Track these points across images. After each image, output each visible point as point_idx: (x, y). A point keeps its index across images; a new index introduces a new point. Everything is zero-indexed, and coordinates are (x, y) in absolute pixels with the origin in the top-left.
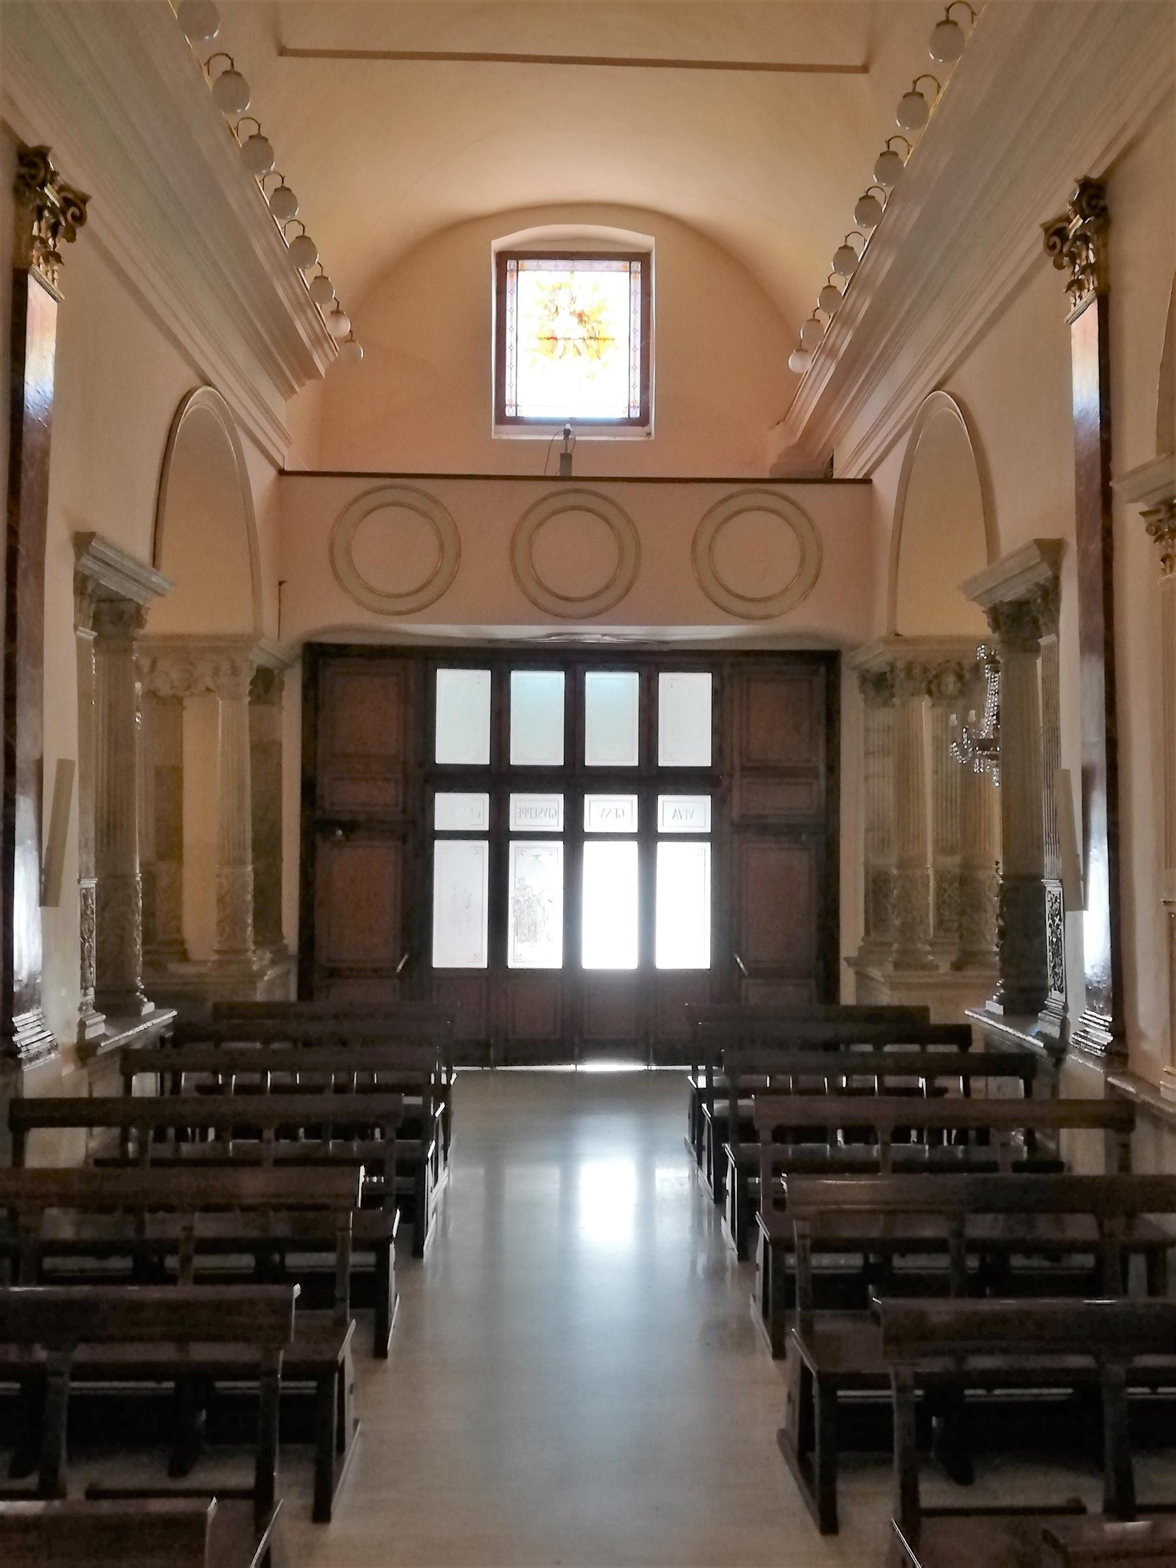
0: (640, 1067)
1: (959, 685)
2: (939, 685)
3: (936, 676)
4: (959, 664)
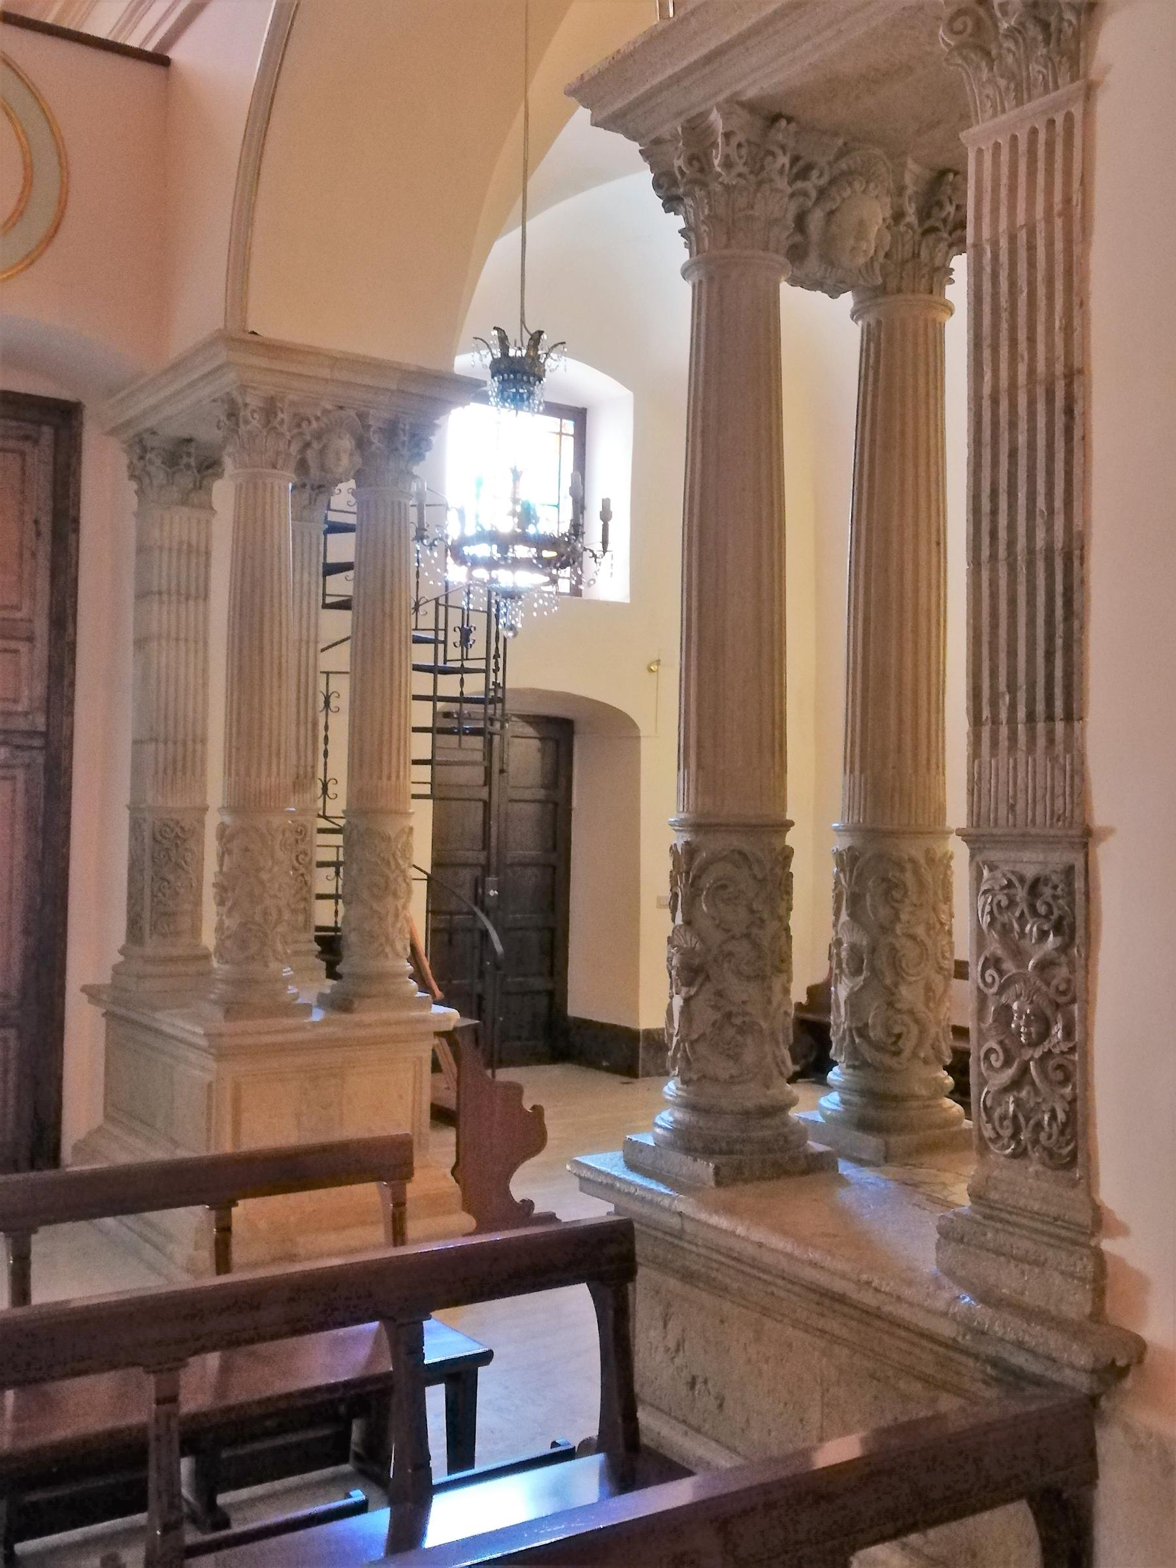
0: (666, 1191)
1: (358, 459)
2: (322, 452)
3: (318, 436)
4: (362, 416)
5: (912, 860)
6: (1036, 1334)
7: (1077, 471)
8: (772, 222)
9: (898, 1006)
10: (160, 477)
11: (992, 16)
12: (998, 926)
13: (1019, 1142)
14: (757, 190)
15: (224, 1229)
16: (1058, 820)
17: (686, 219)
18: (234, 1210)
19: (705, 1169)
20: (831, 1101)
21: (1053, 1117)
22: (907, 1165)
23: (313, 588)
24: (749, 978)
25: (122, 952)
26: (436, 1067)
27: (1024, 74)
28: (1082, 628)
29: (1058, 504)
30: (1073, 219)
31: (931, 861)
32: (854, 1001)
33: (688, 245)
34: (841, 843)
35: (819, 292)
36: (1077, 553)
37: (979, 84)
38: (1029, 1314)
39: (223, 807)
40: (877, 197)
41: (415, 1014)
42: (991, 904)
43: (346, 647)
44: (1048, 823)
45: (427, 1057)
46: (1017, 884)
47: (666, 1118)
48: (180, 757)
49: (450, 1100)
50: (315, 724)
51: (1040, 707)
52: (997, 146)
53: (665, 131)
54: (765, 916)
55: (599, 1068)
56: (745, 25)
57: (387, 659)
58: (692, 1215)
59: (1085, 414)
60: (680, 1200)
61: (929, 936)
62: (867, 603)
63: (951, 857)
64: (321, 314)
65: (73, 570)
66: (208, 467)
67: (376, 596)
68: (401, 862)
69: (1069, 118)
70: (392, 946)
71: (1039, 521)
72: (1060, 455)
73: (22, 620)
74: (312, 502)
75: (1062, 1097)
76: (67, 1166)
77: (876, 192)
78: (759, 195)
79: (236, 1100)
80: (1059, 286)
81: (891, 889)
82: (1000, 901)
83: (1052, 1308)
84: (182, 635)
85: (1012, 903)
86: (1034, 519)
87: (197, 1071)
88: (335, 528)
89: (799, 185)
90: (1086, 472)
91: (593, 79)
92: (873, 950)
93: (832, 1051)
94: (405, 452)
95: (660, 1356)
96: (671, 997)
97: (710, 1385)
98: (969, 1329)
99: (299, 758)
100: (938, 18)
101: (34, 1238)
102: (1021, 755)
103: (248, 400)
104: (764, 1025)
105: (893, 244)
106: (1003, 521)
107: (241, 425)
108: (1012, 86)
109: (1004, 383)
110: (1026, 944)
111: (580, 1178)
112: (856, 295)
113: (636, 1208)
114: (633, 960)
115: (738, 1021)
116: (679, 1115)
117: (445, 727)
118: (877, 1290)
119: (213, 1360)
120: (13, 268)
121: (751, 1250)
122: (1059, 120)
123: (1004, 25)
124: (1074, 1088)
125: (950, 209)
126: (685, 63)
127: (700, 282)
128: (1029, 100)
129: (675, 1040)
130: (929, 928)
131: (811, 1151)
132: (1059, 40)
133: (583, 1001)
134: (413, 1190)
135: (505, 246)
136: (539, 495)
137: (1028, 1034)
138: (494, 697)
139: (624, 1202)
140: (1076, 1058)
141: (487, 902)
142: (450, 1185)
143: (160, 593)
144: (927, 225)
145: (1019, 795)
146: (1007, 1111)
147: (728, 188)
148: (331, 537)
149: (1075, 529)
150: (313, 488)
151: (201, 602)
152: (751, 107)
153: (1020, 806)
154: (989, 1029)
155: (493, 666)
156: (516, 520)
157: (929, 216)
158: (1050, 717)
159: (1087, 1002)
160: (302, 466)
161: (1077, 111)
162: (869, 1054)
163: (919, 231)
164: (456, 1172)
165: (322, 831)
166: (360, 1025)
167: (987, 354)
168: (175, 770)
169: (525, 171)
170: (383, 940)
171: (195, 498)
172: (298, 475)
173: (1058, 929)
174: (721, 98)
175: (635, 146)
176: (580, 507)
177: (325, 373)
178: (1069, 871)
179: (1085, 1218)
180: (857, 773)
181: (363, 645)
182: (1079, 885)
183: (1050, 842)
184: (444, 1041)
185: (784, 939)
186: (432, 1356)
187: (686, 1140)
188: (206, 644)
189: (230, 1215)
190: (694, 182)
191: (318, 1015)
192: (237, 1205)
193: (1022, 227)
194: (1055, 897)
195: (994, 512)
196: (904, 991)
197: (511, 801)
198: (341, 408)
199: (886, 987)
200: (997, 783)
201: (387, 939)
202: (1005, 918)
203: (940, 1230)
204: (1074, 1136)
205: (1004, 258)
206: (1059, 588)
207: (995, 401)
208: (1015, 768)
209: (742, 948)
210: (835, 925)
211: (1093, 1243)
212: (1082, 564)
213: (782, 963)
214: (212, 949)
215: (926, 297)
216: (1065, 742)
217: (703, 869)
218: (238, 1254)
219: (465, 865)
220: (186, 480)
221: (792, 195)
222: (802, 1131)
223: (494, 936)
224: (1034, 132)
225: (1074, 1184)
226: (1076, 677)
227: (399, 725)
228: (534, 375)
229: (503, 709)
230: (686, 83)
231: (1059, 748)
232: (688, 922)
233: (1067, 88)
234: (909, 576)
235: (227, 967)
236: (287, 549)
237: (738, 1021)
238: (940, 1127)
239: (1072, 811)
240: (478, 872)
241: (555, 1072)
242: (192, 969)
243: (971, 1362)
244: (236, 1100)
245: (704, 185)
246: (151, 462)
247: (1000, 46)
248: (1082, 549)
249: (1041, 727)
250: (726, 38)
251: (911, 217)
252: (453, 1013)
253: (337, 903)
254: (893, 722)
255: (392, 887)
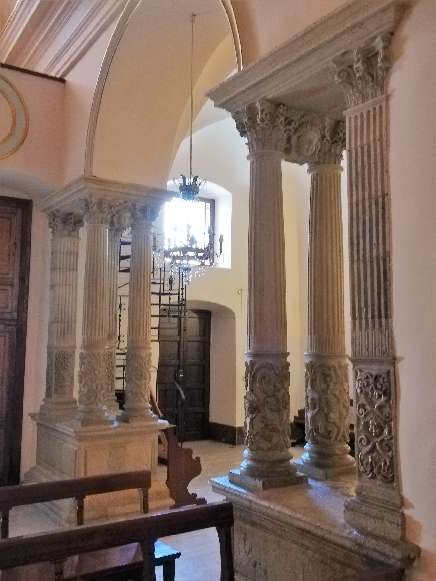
2: (119, 218)
3: (118, 212)
4: (134, 205)
5: (334, 367)
6: (380, 546)
7: (387, 230)
8: (278, 141)
9: (330, 421)
10: (60, 227)
11: (353, 71)
12: (364, 392)
13: (373, 473)
14: (273, 130)
15: (81, 507)
16: (384, 354)
17: (248, 139)
18: (84, 499)
19: (259, 483)
20: (306, 456)
21: (385, 463)
22: (334, 480)
23: (116, 266)
24: (274, 411)
25: (44, 400)
26: (160, 442)
27: (365, 92)
28: (390, 285)
29: (381, 241)
30: (383, 142)
31: (340, 366)
32: (313, 418)
33: (249, 148)
34: (308, 360)
35: (296, 164)
36: (388, 258)
37: (350, 95)
38: (378, 538)
39: (82, 347)
40: (316, 131)
41: (153, 423)
42: (361, 384)
43: (127, 286)
44: (380, 355)
45: (157, 438)
46: (370, 377)
47: (244, 464)
48: (66, 328)
49: (165, 455)
50: (116, 315)
51: (376, 313)
52: (356, 117)
53: (240, 109)
54: (280, 388)
55: (221, 441)
56: (268, 74)
57: (142, 292)
58: (254, 501)
59: (389, 209)
60: (251, 495)
61: (340, 394)
62: (315, 273)
63: (348, 365)
64: (118, 169)
65: (28, 261)
66: (78, 223)
67: (138, 270)
68: (147, 366)
69: (381, 107)
70: (144, 398)
71: (374, 247)
72: (381, 224)
73: (9, 279)
74: (115, 235)
75: (389, 456)
76: (23, 482)
77: (315, 130)
78: (273, 131)
79: (86, 458)
80: (379, 164)
81: (326, 377)
82: (364, 384)
83: (387, 536)
84: (68, 283)
85: (368, 384)
86: (372, 245)
87: (71, 445)
88: (124, 243)
89: (287, 127)
90: (390, 229)
91: (215, 91)
92: (320, 399)
93: (306, 438)
94: (149, 217)
95: (243, 554)
96: (246, 418)
97: (261, 565)
98: (357, 544)
99: (110, 328)
100: (335, 72)
101: (10, 511)
102: (370, 330)
103: (93, 200)
104: (280, 429)
105: (322, 147)
106: (361, 247)
107: (90, 209)
108: (361, 96)
109: (360, 198)
110: (373, 399)
111: (212, 486)
112: (309, 164)
113: (233, 498)
114: (232, 405)
115: (270, 427)
116: (249, 462)
117: (165, 313)
118: (322, 529)
119: (76, 558)
120: (7, 154)
121: (276, 514)
122: (378, 107)
123: (358, 75)
124: (392, 452)
125: (341, 134)
126: (247, 86)
127: (253, 161)
128: (367, 101)
129: (247, 434)
130: (340, 391)
131: (298, 476)
132: (376, 81)
133: (216, 416)
134: (150, 491)
135: (186, 142)
136: (198, 228)
137: (375, 433)
138: (182, 304)
139: (229, 495)
140: (393, 441)
141: (179, 379)
142: (165, 488)
143: (60, 268)
144: (334, 140)
145: (370, 345)
146: (368, 462)
147: (263, 129)
148: (122, 247)
149: (387, 250)
150: (116, 230)
151: (75, 272)
152: (270, 101)
153: (370, 349)
154: (361, 430)
155: (181, 292)
156: (189, 242)
157: (334, 137)
158: (380, 317)
159: (396, 421)
160: (112, 223)
161: (384, 105)
162: (319, 439)
163: (331, 142)
164: (168, 483)
165: (118, 354)
166: (133, 428)
167: (354, 187)
168: (64, 333)
169: (192, 119)
170: (140, 395)
171: (73, 234)
172: (110, 226)
173: (385, 394)
174: (260, 98)
175: (230, 114)
176: (212, 235)
177: (120, 190)
178: (388, 373)
179: (398, 502)
180: (313, 334)
181: (133, 295)
182: (392, 378)
183: (380, 362)
184: (163, 433)
185: (287, 395)
186: (158, 555)
187: (252, 472)
188: (76, 286)
189: (83, 501)
190: (251, 127)
191: (116, 424)
192: (85, 498)
193: (365, 144)
194: (384, 382)
195: (358, 243)
196: (332, 415)
197: (189, 341)
198: (126, 202)
199: (325, 414)
200: (362, 340)
201: (142, 395)
202: (366, 390)
203: (345, 505)
204: (393, 470)
205: (359, 154)
206: (382, 271)
207: (357, 205)
208: (368, 335)
209: (271, 400)
210: (306, 390)
211: (401, 511)
212: (389, 262)
213: (286, 405)
214: (77, 399)
215: (334, 165)
216: (385, 326)
217: (257, 370)
218: (86, 515)
219: (171, 366)
220: (70, 228)
221: (285, 131)
222: (295, 468)
223: (182, 392)
224: (369, 112)
225: (393, 489)
226: (389, 303)
227: (147, 316)
228: (195, 191)
229: (185, 308)
230: (247, 93)
231: (384, 327)
232: (252, 390)
233: (380, 97)
234: (330, 264)
235: (82, 406)
236: (106, 252)
237: (270, 427)
238: (346, 466)
239: (389, 351)
240: (176, 368)
241: (205, 443)
242: (70, 406)
243: (357, 556)
244: (86, 458)
245: (254, 128)
246: (57, 222)
247: (356, 82)
248: (389, 257)
249: (377, 320)
250: (261, 78)
251: (328, 137)
252: (166, 422)
253: (123, 381)
254: (325, 316)
255: (144, 375)
